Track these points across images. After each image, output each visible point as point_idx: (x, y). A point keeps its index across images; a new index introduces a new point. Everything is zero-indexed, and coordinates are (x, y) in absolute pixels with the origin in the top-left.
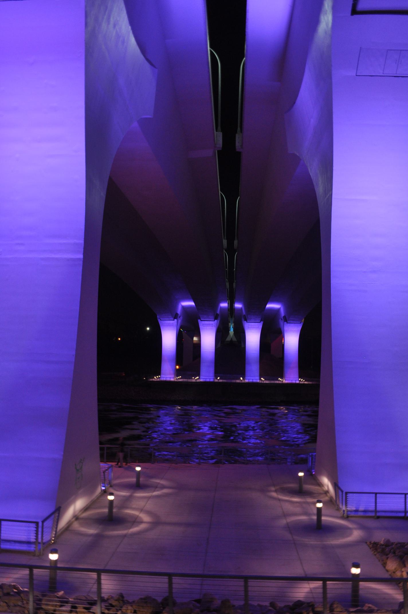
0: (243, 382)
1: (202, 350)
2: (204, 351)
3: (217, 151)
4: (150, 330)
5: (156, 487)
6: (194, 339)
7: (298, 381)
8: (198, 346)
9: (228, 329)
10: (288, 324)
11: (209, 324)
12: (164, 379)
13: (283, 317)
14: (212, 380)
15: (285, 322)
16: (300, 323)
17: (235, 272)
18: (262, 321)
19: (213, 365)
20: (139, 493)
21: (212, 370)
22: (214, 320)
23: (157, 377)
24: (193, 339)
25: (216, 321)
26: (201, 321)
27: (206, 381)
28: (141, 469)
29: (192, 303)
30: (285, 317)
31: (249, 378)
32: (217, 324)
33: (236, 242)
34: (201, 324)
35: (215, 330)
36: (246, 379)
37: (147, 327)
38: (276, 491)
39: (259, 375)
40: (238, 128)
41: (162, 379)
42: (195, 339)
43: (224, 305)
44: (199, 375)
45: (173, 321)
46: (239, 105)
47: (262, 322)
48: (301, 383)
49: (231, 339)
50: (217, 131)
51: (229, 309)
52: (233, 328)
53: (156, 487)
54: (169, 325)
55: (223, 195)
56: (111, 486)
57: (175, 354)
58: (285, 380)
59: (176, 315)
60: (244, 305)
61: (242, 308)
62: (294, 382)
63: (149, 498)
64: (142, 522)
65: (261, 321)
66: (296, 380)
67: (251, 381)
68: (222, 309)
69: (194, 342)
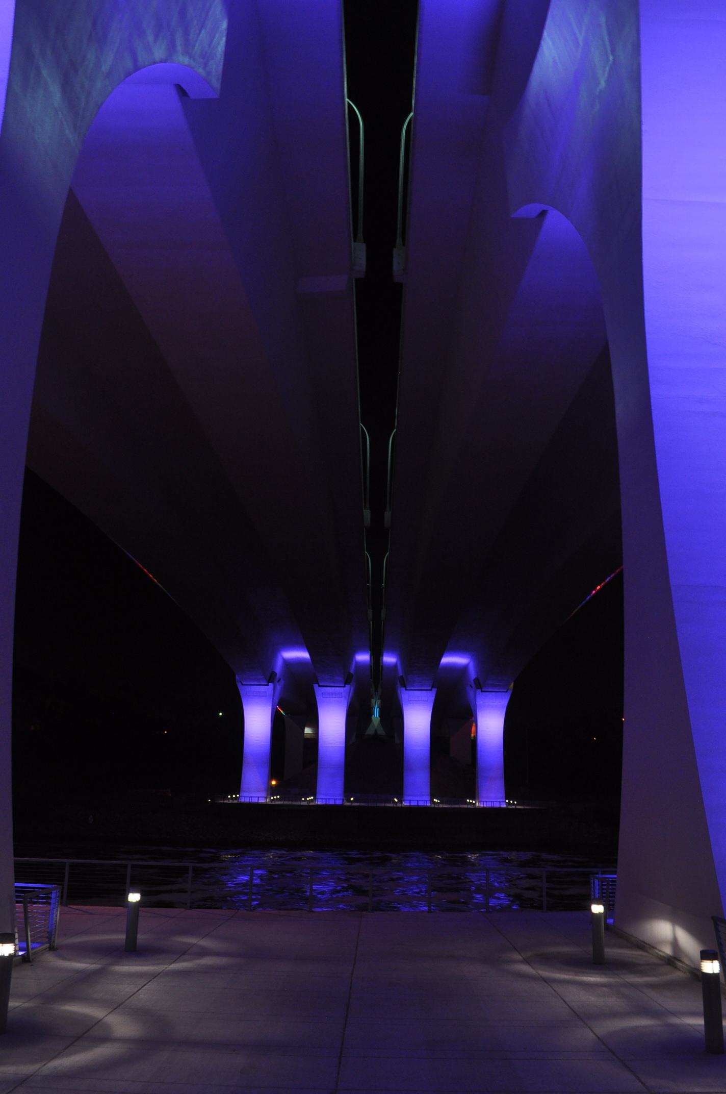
0: (399, 805)
3: (354, 279)
5: (184, 953)
6: (305, 732)
7: (505, 803)
8: (314, 742)
9: (371, 713)
10: (407, 691)
11: (335, 693)
12: (247, 800)
13: (474, 680)
14: (339, 802)
15: (478, 688)
16: (507, 692)
17: (384, 590)
18: (435, 688)
20: (126, 965)
21: (339, 783)
22: (343, 686)
23: (511, 802)
24: (304, 731)
25: (348, 687)
26: (319, 686)
27: (328, 803)
28: (142, 895)
29: (304, 655)
30: (477, 680)
31: (409, 798)
32: (349, 693)
33: (388, 515)
34: (319, 691)
35: (346, 709)
36: (404, 800)
37: (220, 713)
38: (527, 961)
39: (429, 794)
40: (398, 240)
41: (243, 800)
42: (308, 731)
43: (363, 657)
44: (314, 795)
45: (344, 688)
46: (399, 205)
47: (434, 691)
48: (509, 807)
49: (376, 731)
50: (355, 241)
51: (371, 666)
52: (378, 709)
53: (181, 953)
55: (367, 433)
56: (52, 949)
57: (269, 747)
58: (480, 802)
59: (271, 675)
60: (401, 658)
61: (396, 665)
62: (497, 805)
63: (154, 976)
64: (105, 1039)
65: (432, 687)
66: (500, 802)
67: (414, 804)
68: (359, 665)
69: (306, 736)
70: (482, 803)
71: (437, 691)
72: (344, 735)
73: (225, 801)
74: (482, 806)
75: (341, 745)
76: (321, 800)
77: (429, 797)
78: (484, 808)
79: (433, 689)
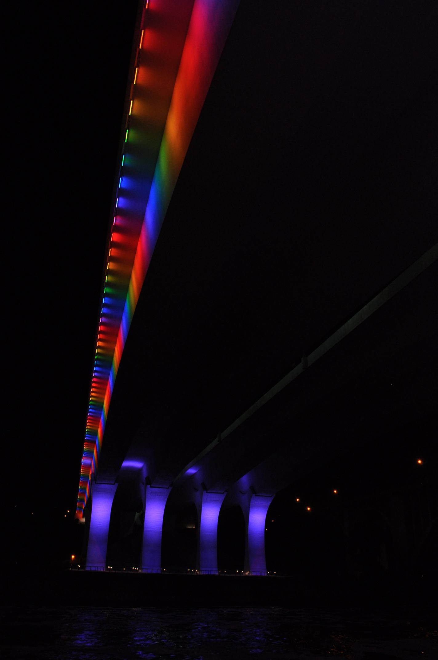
47: (117, 484)
48: (163, 573)
62: (212, 573)
73: (130, 572)
75: (160, 530)
76: (100, 568)
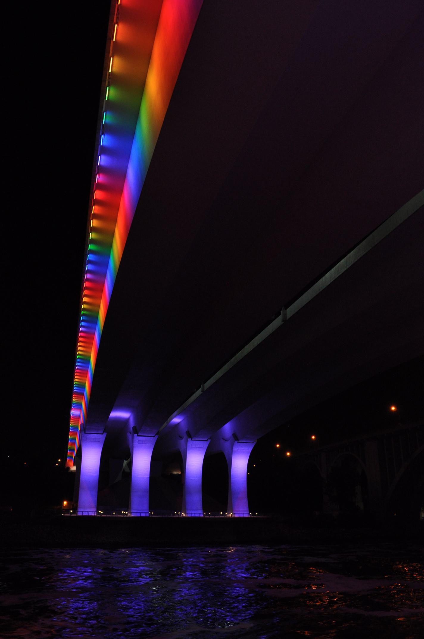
1: (81, 476)
2: (137, 476)
4: (286, 454)
10: (192, 441)
15: (236, 440)
19: (147, 494)
27: (195, 516)
39: (202, 509)
47: (105, 434)
54: (94, 441)
58: (185, 513)
65: (104, 432)
70: (188, 514)
71: (107, 434)
72: (149, 469)
74: (132, 515)
77: (202, 511)
78: (189, 518)
79: (104, 433)
